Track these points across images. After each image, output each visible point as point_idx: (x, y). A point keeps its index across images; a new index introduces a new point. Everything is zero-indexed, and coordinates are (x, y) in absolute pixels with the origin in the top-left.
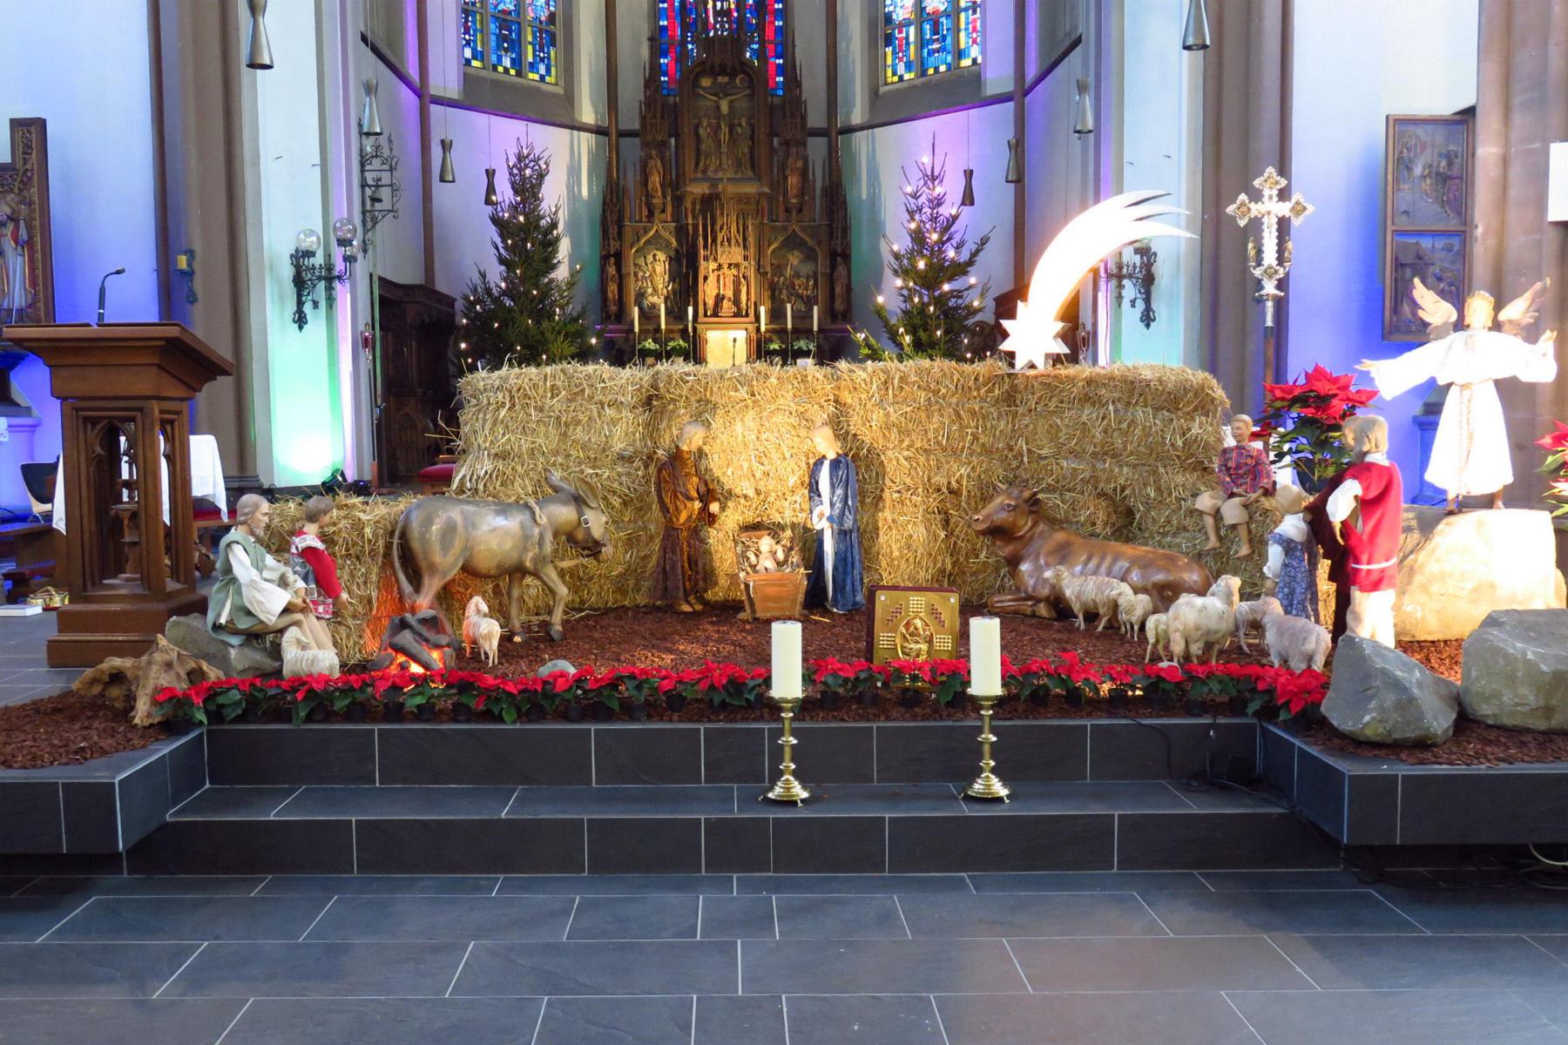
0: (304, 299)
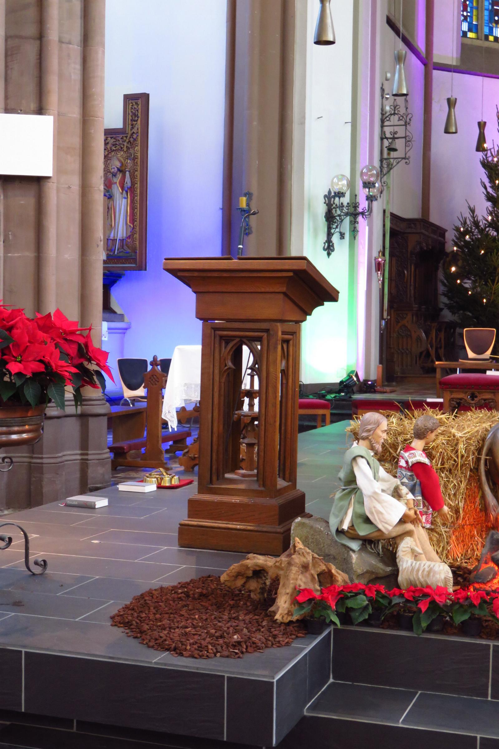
0: (333, 231)
